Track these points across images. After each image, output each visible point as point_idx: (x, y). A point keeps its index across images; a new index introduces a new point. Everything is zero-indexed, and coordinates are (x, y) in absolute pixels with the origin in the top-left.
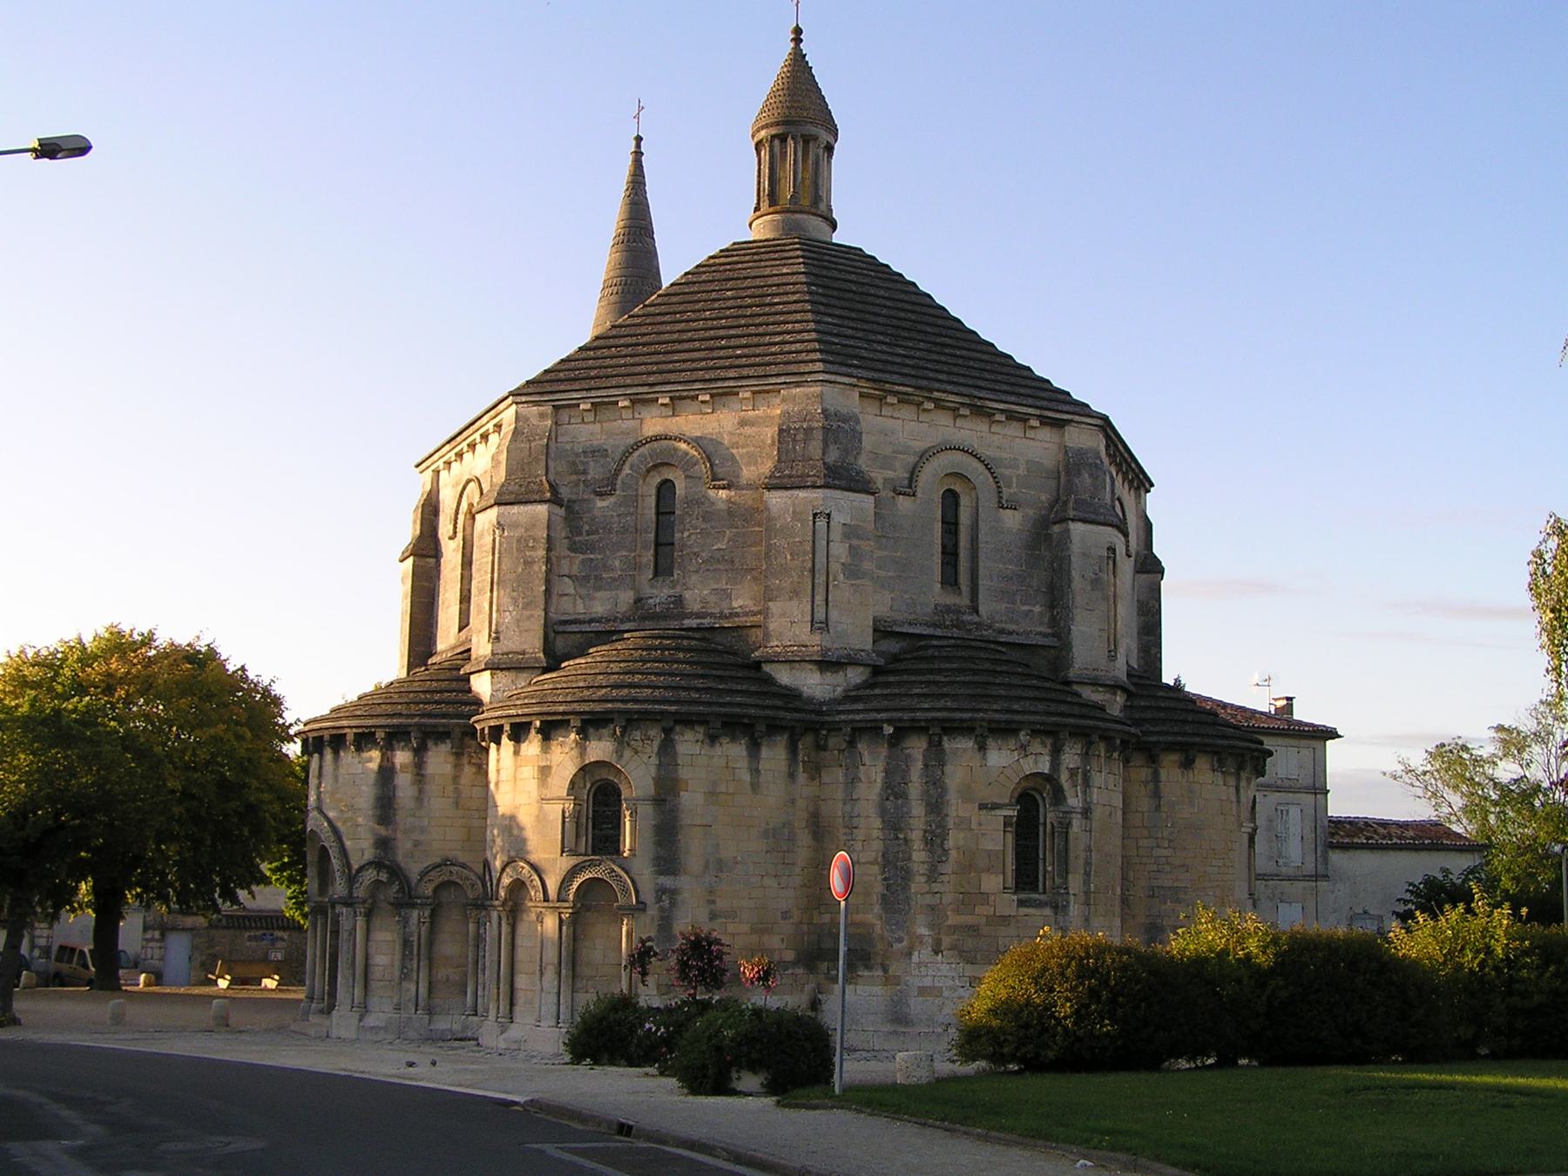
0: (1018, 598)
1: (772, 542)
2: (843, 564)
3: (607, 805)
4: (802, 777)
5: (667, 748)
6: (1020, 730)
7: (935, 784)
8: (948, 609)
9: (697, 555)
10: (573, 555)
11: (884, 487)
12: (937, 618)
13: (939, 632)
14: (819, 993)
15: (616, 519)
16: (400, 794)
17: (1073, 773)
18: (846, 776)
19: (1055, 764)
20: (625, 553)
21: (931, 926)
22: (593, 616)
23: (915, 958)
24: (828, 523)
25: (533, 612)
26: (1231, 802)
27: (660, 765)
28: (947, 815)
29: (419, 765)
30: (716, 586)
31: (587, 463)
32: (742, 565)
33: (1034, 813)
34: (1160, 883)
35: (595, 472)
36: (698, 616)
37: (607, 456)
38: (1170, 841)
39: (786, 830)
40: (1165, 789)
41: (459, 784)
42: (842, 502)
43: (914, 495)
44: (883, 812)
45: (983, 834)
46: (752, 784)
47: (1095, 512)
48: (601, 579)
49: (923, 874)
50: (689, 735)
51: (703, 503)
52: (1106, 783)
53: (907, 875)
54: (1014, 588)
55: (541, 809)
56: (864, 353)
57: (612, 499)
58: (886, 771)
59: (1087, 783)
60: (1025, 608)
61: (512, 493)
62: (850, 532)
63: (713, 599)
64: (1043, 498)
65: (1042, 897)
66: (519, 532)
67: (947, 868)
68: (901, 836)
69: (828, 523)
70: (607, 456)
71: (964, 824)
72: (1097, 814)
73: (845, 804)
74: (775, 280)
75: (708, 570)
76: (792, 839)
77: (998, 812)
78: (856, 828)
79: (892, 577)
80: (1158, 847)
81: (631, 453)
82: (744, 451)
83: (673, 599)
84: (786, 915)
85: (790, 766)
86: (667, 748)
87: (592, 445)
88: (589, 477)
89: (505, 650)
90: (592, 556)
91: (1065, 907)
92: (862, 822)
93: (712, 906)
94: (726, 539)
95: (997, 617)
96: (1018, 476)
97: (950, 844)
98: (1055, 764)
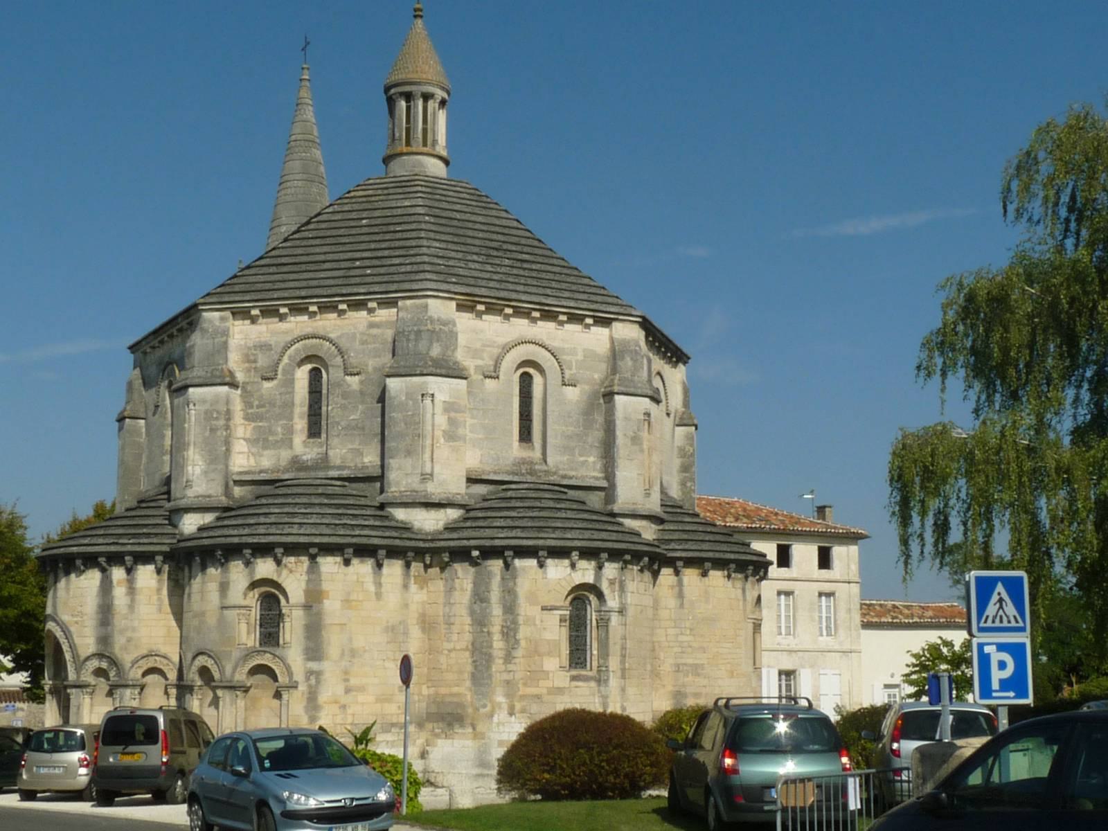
0: (577, 451)
2: (443, 431)
3: (270, 610)
5: (314, 568)
7: (509, 592)
8: (523, 461)
9: (338, 423)
10: (246, 423)
11: (475, 373)
12: (515, 468)
13: (516, 479)
14: (427, 745)
15: (278, 397)
17: (612, 582)
18: (445, 586)
19: (598, 576)
20: (285, 422)
21: (508, 695)
22: (262, 468)
23: (495, 719)
24: (432, 401)
26: (738, 600)
27: (308, 581)
28: (518, 615)
29: (131, 582)
30: (350, 447)
33: (584, 613)
34: (683, 661)
35: (263, 361)
36: (339, 468)
37: (271, 349)
38: (691, 630)
39: (402, 627)
40: (686, 590)
43: (498, 378)
44: (472, 613)
46: (376, 594)
47: (635, 387)
49: (501, 658)
50: (330, 559)
52: (637, 589)
53: (489, 659)
55: (222, 614)
56: (461, 272)
57: (275, 382)
58: (475, 584)
59: (622, 589)
60: (582, 459)
61: (199, 377)
62: (449, 407)
63: (350, 456)
64: (596, 376)
65: (590, 674)
66: (207, 406)
67: (519, 653)
68: (485, 630)
69: (432, 401)
70: (271, 349)
71: (530, 621)
72: (631, 611)
73: (445, 606)
74: (399, 211)
76: (406, 633)
77: (555, 612)
78: (453, 624)
79: (481, 439)
81: (289, 348)
82: (373, 346)
85: (404, 579)
86: (314, 568)
87: (260, 342)
89: (196, 494)
90: (260, 424)
91: (606, 681)
93: (347, 683)
94: (359, 412)
95: (561, 466)
97: (520, 635)
98: (598, 576)
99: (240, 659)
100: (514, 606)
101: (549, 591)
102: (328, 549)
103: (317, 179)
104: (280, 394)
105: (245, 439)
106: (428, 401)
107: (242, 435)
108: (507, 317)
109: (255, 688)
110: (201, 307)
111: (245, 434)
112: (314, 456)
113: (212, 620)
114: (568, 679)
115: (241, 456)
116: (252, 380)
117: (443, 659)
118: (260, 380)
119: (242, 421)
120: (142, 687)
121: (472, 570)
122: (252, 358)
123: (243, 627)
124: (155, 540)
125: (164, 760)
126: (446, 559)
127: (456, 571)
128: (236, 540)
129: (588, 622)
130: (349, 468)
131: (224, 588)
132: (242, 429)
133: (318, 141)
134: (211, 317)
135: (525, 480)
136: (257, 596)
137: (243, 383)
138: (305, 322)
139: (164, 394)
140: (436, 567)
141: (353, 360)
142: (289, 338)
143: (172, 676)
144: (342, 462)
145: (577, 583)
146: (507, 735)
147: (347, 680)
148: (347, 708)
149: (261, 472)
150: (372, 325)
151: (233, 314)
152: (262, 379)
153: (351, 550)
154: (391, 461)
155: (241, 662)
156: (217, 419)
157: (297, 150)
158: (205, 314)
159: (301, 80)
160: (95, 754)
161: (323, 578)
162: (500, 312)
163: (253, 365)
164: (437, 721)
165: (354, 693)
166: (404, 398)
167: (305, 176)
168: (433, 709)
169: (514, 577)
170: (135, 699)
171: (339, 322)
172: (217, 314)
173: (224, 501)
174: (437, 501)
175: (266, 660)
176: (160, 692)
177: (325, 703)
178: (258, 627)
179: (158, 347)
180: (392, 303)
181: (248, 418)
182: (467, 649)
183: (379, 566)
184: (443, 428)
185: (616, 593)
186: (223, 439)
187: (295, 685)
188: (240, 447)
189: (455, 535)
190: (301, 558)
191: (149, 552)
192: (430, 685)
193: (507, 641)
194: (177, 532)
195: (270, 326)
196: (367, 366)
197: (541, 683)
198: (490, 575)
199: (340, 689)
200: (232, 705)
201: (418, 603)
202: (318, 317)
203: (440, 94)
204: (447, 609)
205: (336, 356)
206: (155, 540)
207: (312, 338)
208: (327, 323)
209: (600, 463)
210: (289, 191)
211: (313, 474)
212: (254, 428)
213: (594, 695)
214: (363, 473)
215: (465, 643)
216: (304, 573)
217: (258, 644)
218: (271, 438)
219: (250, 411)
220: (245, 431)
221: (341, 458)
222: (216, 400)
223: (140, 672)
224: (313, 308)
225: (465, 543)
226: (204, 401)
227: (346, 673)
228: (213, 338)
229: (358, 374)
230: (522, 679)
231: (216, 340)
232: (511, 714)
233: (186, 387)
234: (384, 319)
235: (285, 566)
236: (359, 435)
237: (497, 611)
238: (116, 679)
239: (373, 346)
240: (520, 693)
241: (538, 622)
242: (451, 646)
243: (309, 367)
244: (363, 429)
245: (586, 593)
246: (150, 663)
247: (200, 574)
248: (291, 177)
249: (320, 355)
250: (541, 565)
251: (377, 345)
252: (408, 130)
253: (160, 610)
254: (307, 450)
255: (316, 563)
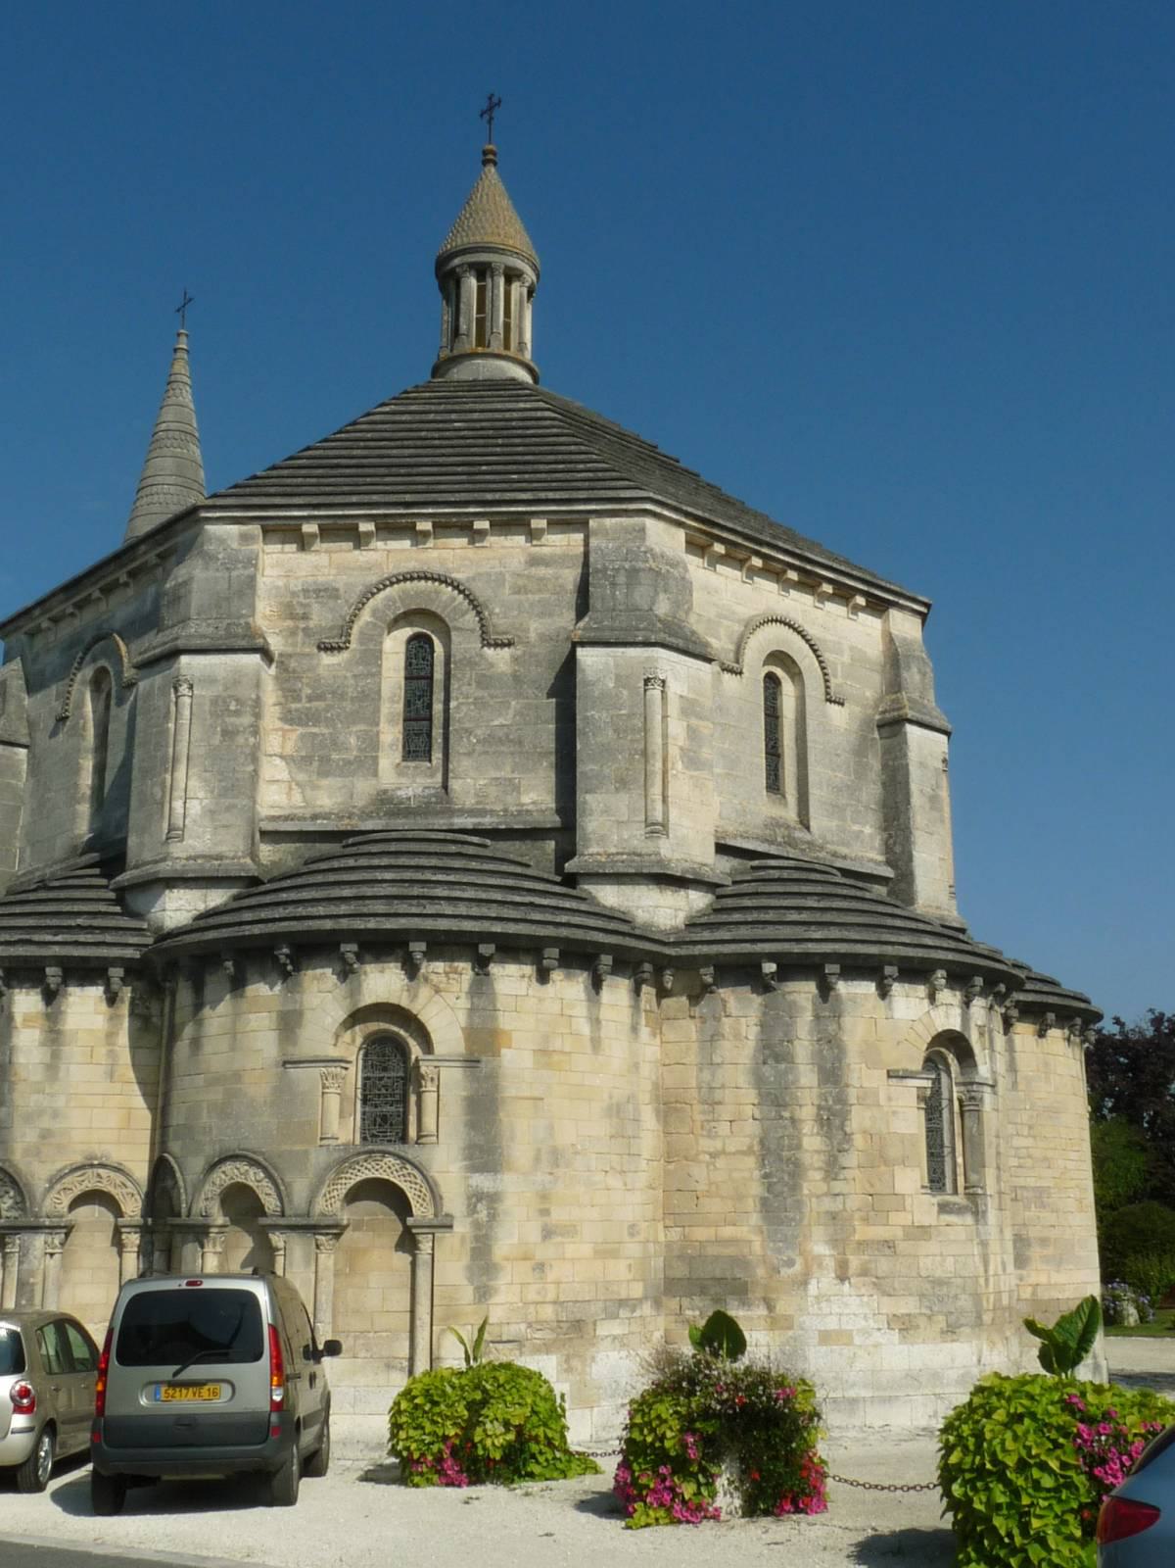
1: (589, 714)
2: (681, 749)
3: (385, 1069)
4: (645, 1031)
6: (933, 971)
7: (830, 1042)
10: (287, 727)
12: (768, 832)
13: (773, 850)
15: (352, 682)
16: (20, 1059)
18: (701, 1031)
19: (965, 1019)
21: (833, 1242)
22: (318, 810)
23: (813, 1288)
25: (236, 801)
27: (472, 1010)
28: (847, 1086)
30: (498, 775)
31: (308, 605)
32: (535, 747)
34: (1021, 1182)
35: (321, 617)
36: (472, 812)
37: (337, 597)
38: (1030, 1127)
41: (114, 1044)
42: (678, 667)
43: (741, 673)
44: (759, 1081)
45: (894, 1113)
48: (329, 760)
49: (820, 1169)
50: (512, 969)
51: (476, 664)
53: (796, 1170)
54: (844, 802)
57: (345, 655)
58: (762, 1025)
60: (856, 828)
61: (204, 636)
62: (689, 708)
63: (493, 791)
66: (217, 690)
67: (851, 1159)
68: (786, 1114)
70: (337, 597)
71: (868, 1098)
75: (487, 753)
78: (720, 1103)
80: (1018, 1135)
81: (373, 594)
82: (537, 597)
83: (433, 791)
84: (633, 1230)
87: (315, 583)
88: (311, 624)
90: (315, 730)
92: (728, 1095)
93: (545, 1219)
94: (511, 712)
95: (829, 837)
96: (843, 663)
99: (328, 1168)
100: (840, 1068)
101: (898, 1043)
102: (512, 948)
103: (196, 486)
104: (355, 676)
105: (282, 757)
106: (655, 693)
107: (278, 750)
108: (753, 572)
109: (354, 1230)
110: (204, 514)
111: (283, 747)
112: (419, 791)
113: (258, 1087)
114: (936, 1208)
115: (274, 787)
116: (298, 650)
117: (699, 1172)
118: (316, 650)
119: (279, 724)
120: (69, 1230)
121: (757, 1000)
122: (300, 611)
123: (333, 1102)
124: (108, 938)
125: (277, 1398)
126: (709, 979)
127: (724, 1002)
128: (328, 925)
129: (945, 1103)
130: (492, 812)
131: (289, 1023)
132: (277, 739)
133: (197, 434)
134: (223, 534)
135: (785, 855)
136: (359, 1040)
137: (281, 655)
138: (403, 550)
139: (83, 694)
140: (682, 995)
141: (501, 620)
142: (373, 579)
143: (133, 1207)
144: (478, 803)
145: (940, 1030)
146: (835, 1318)
147: (545, 1212)
148: (547, 1268)
149: (315, 817)
150: (534, 561)
151: (266, 531)
152: (319, 648)
153: (554, 952)
154: (588, 797)
155: (331, 1175)
156: (237, 713)
157: (169, 443)
158: (210, 528)
159: (176, 350)
160: (100, 1387)
161: (499, 1006)
162: (740, 563)
163: (302, 625)
164: (690, 1295)
165: (559, 1239)
166: (611, 685)
167: (180, 480)
168: (680, 1271)
169: (837, 1015)
170: (52, 1255)
171: (471, 552)
172: (234, 529)
173: (248, 867)
174: (679, 874)
175: (386, 1169)
176: (104, 1239)
177: (507, 1259)
178: (359, 1103)
179: (72, 615)
180: (577, 523)
181: (289, 718)
182: (749, 1152)
183: (597, 984)
184: (680, 744)
185: (987, 1051)
186: (247, 751)
187: (447, 1222)
188: (273, 770)
189: (706, 935)
190: (456, 964)
191: (97, 958)
192: (669, 1223)
193: (828, 1136)
194: (145, 926)
195: (334, 556)
196: (527, 630)
197: (894, 1217)
198: (792, 1010)
199: (533, 1233)
200: (308, 1264)
201: (650, 1062)
202: (431, 543)
203: (530, 276)
204: (706, 1075)
205: (466, 612)
206: (108, 938)
207: (419, 578)
208: (445, 553)
209: (879, 837)
210: (156, 498)
211: (421, 822)
212: (302, 737)
213: (972, 1240)
214: (524, 823)
215: (747, 1141)
216: (463, 995)
217: (358, 1141)
218: (335, 756)
219: (293, 706)
220: (284, 742)
221: (477, 795)
222: (236, 679)
223: (66, 1200)
224: (425, 526)
225: (747, 948)
226: (211, 680)
227: (544, 1197)
228: (228, 569)
229: (509, 644)
230: (859, 1210)
231: (234, 574)
232: (842, 1278)
233: (175, 654)
234: (558, 551)
235: (426, 979)
236: (512, 754)
237: (807, 1077)
238: (14, 1214)
239: (537, 597)
240: (857, 1237)
241: (883, 1101)
242: (718, 1145)
243: (407, 632)
244: (520, 743)
245: (943, 1050)
246: (88, 1182)
247: (228, 997)
248: (159, 479)
249: (433, 609)
250: (884, 993)
251: (546, 596)
252: (481, 323)
253: (111, 1076)
254: (403, 780)
255: (487, 974)
